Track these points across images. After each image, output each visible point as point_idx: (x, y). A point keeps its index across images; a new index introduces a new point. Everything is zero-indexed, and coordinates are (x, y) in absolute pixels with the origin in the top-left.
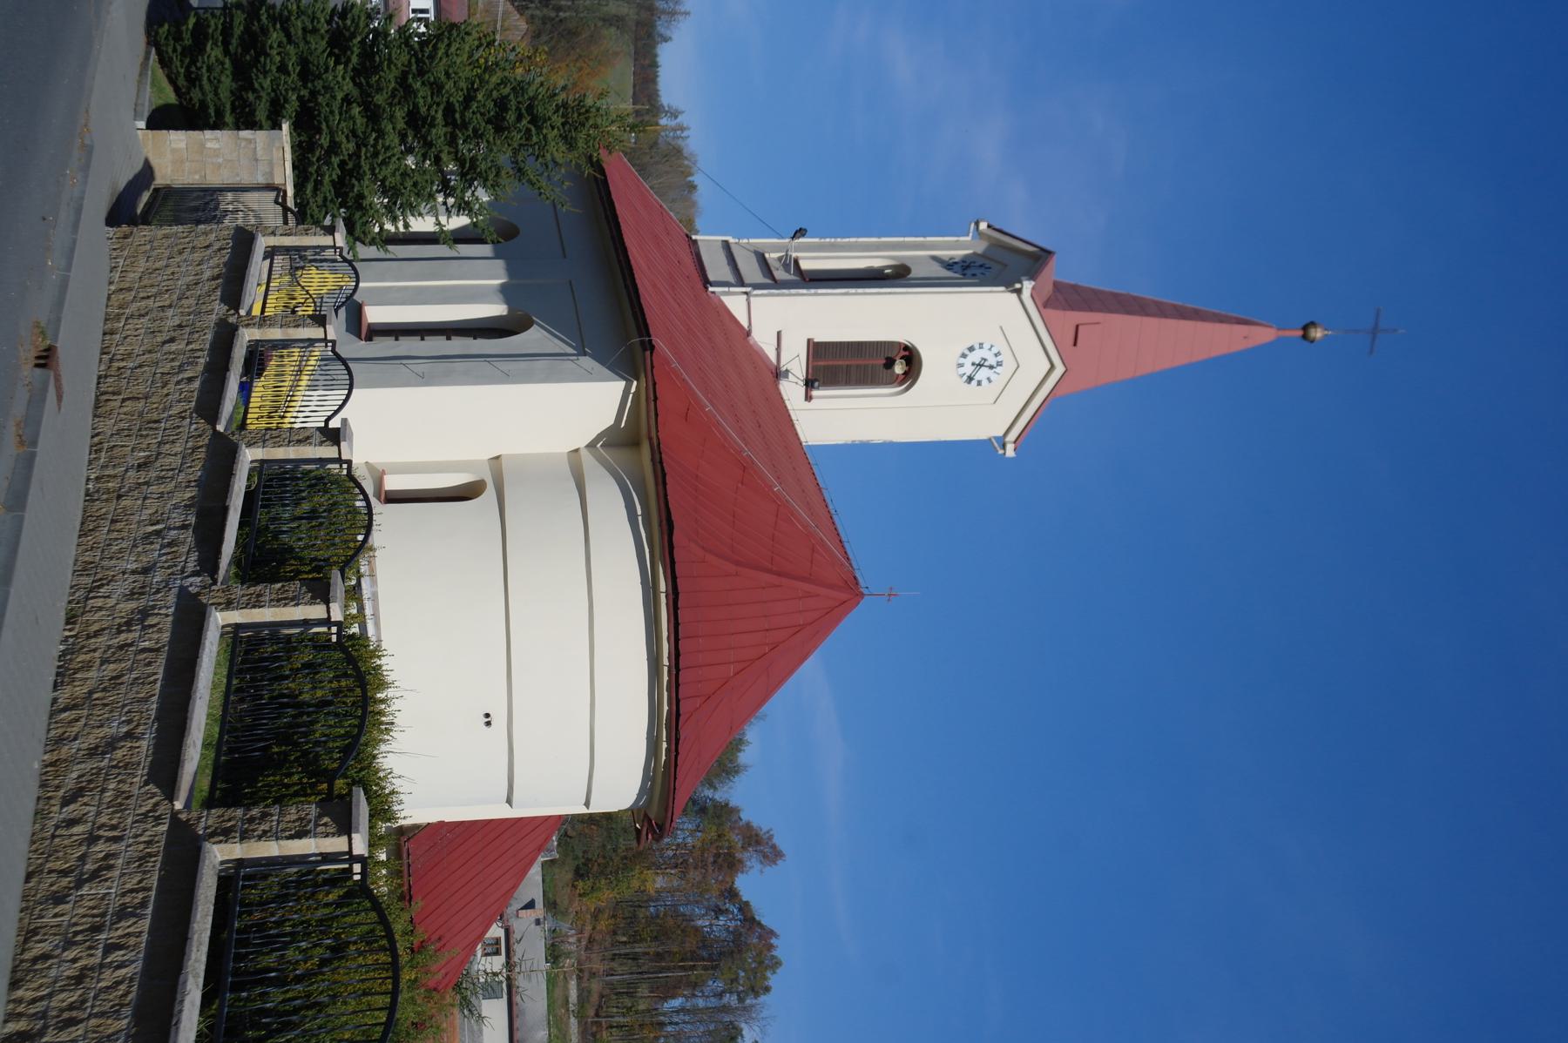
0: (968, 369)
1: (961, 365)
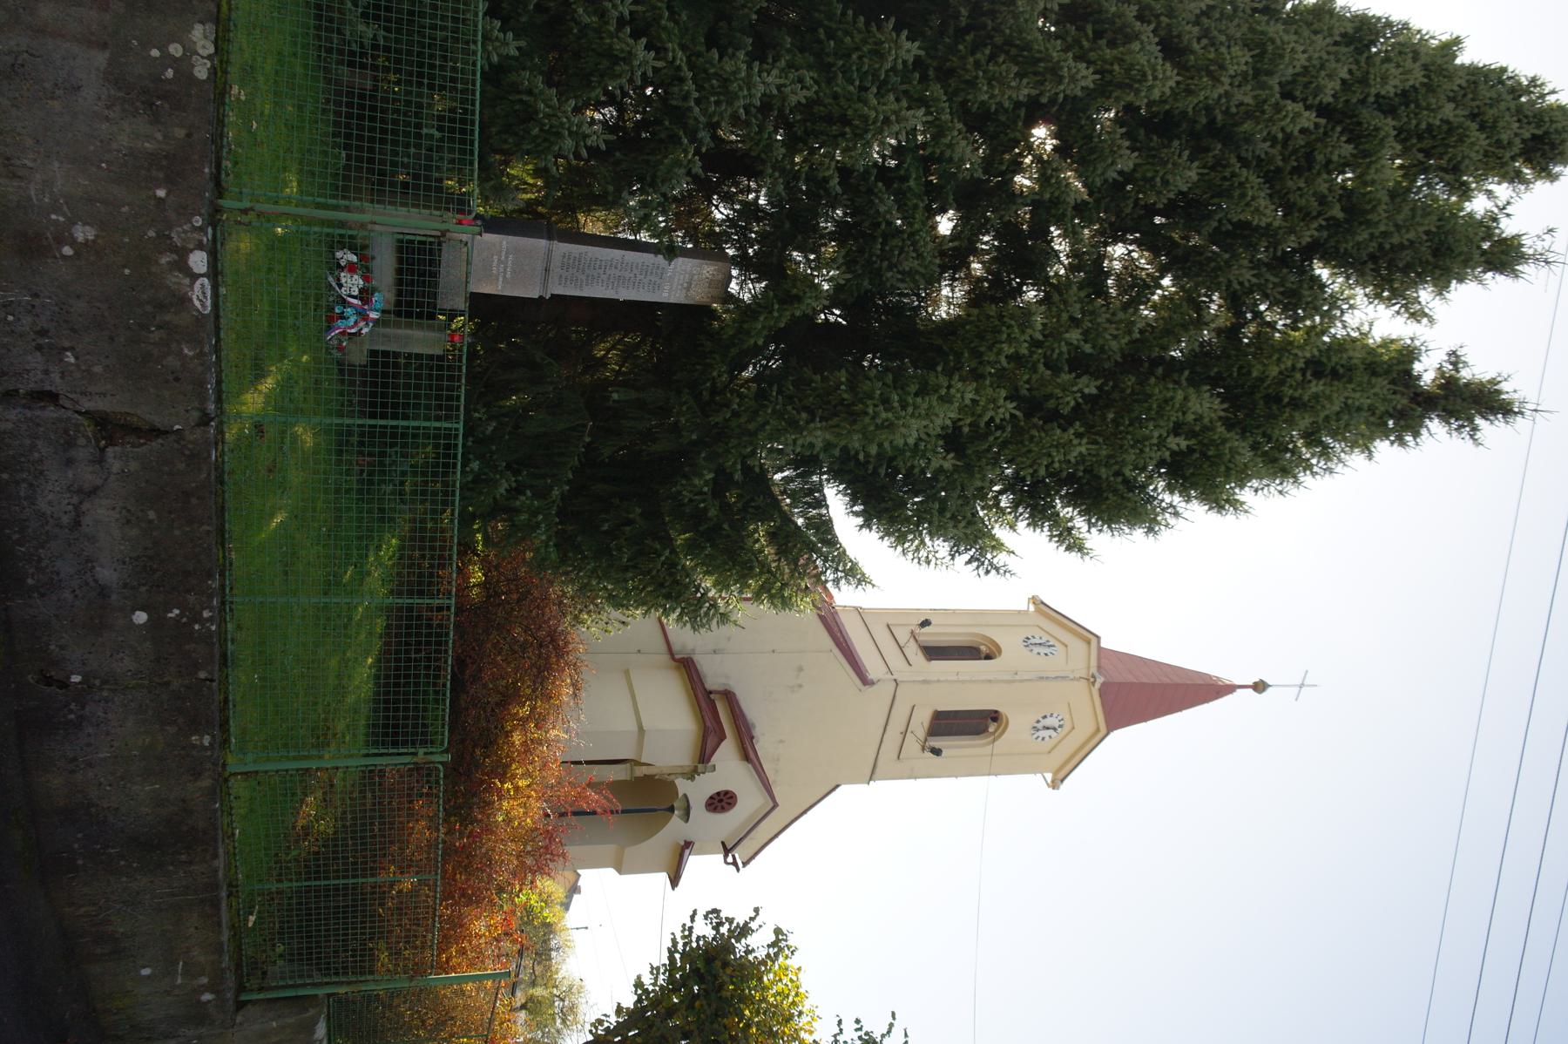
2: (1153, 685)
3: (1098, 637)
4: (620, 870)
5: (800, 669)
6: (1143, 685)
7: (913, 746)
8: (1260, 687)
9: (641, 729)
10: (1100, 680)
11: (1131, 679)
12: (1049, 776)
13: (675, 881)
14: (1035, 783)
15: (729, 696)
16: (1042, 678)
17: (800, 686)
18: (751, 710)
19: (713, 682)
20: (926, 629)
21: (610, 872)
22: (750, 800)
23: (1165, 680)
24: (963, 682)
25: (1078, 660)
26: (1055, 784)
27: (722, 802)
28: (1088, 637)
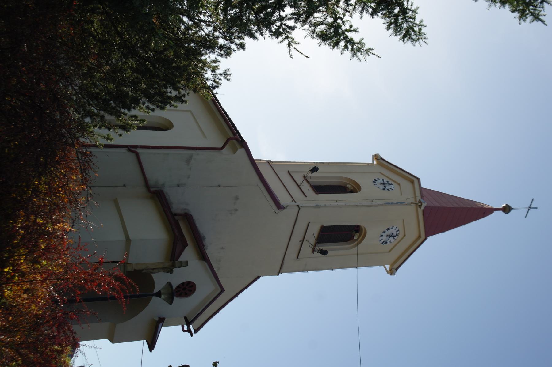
0: (384, 238)
1: (382, 236)
2: (450, 209)
3: (418, 179)
4: (113, 341)
5: (237, 198)
6: (445, 208)
7: (307, 249)
8: (507, 209)
9: (128, 240)
10: (424, 205)
11: (437, 205)
12: (388, 267)
13: (151, 347)
14: (380, 271)
15: (188, 218)
16: (388, 204)
17: (236, 210)
18: (203, 227)
19: (177, 207)
20: (315, 174)
21: (105, 342)
22: (205, 289)
23: (456, 205)
24: (340, 207)
25: (407, 193)
26: (392, 272)
27: (187, 289)
28: (413, 180)
